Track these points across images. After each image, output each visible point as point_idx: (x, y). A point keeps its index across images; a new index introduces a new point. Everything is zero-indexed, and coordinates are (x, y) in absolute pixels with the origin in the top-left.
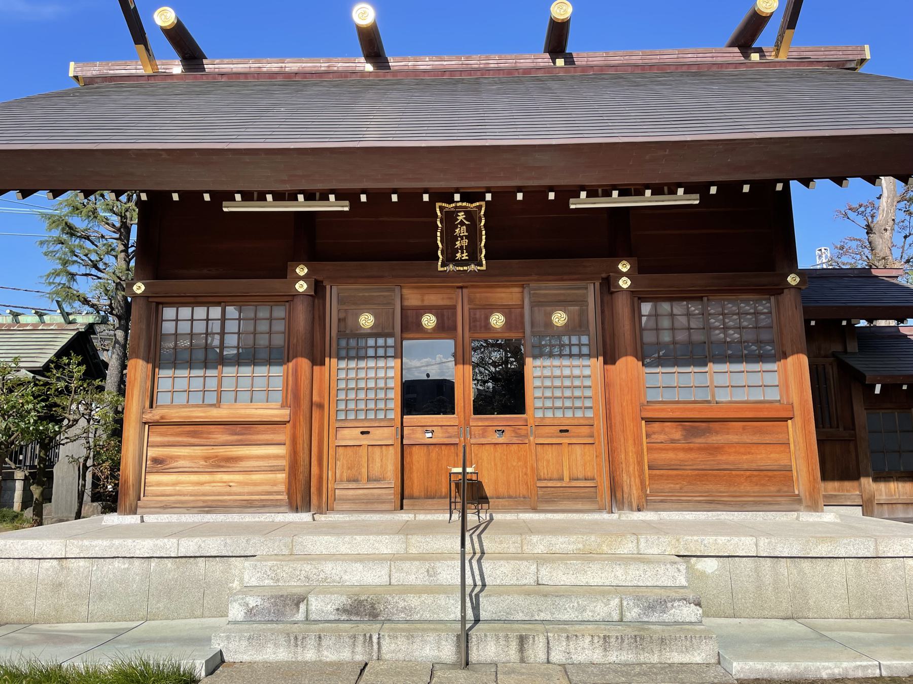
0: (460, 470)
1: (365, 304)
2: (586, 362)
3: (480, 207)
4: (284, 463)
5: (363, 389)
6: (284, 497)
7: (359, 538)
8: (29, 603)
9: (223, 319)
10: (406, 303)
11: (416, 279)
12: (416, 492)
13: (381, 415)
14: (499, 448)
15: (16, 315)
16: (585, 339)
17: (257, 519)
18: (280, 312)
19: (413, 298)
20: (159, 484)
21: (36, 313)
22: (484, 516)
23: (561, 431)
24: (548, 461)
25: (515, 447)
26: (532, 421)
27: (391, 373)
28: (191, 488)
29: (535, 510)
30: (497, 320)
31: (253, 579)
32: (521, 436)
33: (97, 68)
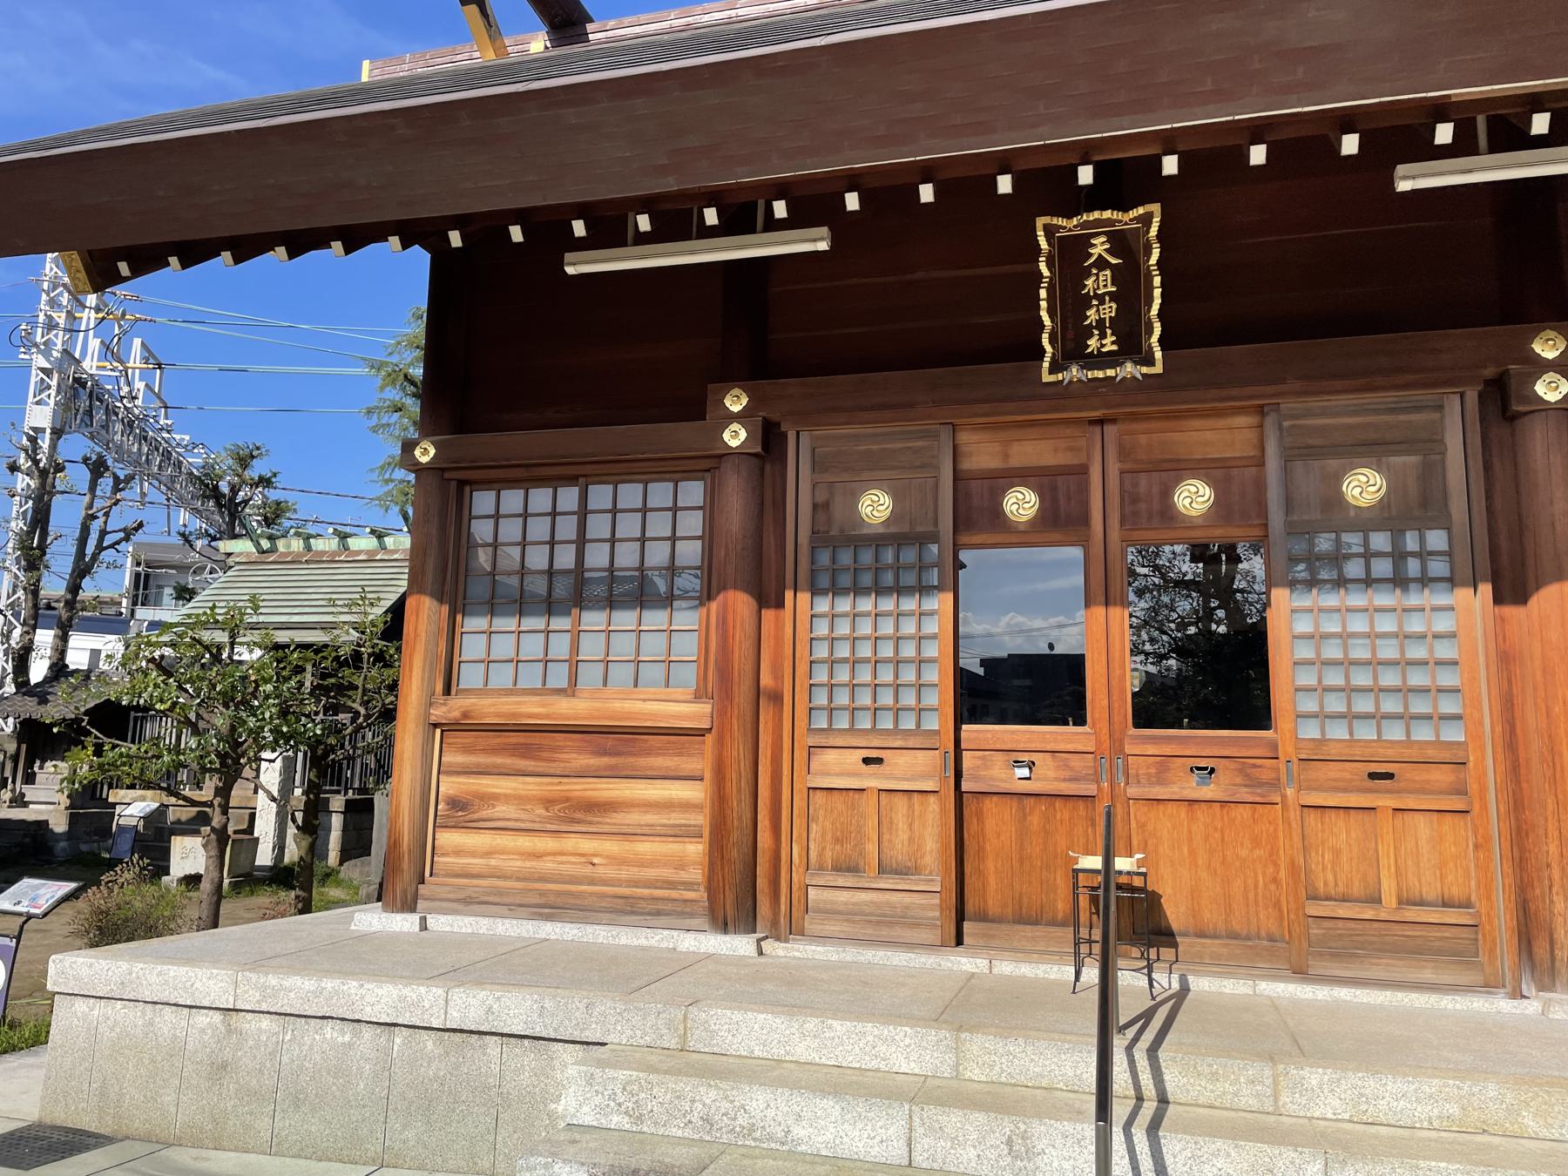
0: (1095, 862)
1: (872, 470)
2: (1443, 599)
3: (1146, 220)
4: (701, 820)
5: (866, 661)
6: (700, 895)
7: (839, 1026)
8: (169, 1098)
9: (583, 513)
10: (967, 465)
11: (987, 407)
12: (993, 907)
13: (908, 723)
14: (1201, 813)
15: (344, 537)
16: (1437, 539)
17: (643, 942)
18: (693, 492)
19: (983, 453)
20: (458, 852)
21: (373, 532)
22: (1166, 981)
23: (1373, 776)
24: (1337, 853)
25: (1242, 813)
26: (1290, 749)
27: (931, 627)
28: (516, 864)
29: (1300, 973)
30: (1194, 497)
31: (586, 1109)
32: (1261, 784)
33: (406, 67)
